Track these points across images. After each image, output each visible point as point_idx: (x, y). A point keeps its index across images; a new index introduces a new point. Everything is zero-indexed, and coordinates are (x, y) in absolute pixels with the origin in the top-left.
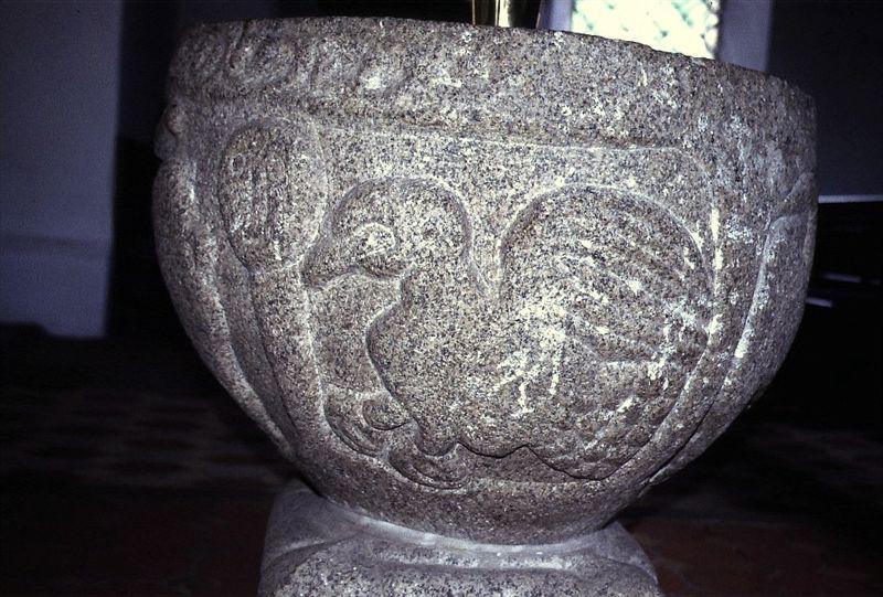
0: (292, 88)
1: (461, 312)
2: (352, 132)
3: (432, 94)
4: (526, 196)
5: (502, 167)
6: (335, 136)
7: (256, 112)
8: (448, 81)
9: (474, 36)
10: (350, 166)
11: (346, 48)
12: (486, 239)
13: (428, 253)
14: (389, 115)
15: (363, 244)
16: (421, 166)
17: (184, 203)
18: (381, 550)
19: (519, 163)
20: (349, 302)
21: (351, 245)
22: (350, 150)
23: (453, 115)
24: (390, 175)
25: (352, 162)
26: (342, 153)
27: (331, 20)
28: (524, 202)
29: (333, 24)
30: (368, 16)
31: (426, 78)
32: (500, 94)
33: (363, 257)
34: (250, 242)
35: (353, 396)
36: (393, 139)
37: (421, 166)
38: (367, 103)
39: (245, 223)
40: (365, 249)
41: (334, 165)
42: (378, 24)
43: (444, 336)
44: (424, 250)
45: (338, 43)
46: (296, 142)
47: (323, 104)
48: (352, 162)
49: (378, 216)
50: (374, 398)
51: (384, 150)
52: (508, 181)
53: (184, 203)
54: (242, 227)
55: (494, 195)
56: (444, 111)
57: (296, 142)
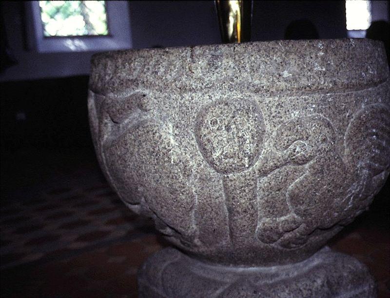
0: (240, 81)
1: (337, 172)
2: (277, 99)
3: (315, 76)
4: (353, 115)
5: (343, 104)
6: (267, 102)
7: (128, 94)
8: (319, 68)
9: (323, 45)
10: (279, 115)
11: (264, 57)
12: (340, 137)
13: (323, 149)
14: (299, 89)
15: (294, 152)
16: (312, 109)
17: (169, 146)
18: (257, 281)
19: (349, 101)
20: (282, 179)
21: (288, 153)
22: (277, 107)
23: (326, 84)
24: (298, 116)
25: (279, 113)
26: (273, 109)
27: (252, 44)
28: (352, 118)
29: (253, 46)
30: (271, 41)
31: (311, 69)
32: (341, 71)
33: (294, 157)
34: (227, 161)
35: (276, 221)
36: (298, 99)
37: (312, 109)
38: (287, 84)
39: (223, 152)
40: (295, 154)
41: (269, 116)
42: (278, 44)
43: (329, 184)
44: (322, 148)
45: (260, 56)
46: (251, 108)
47: (263, 87)
48: (279, 113)
49: (301, 137)
50: (287, 219)
51: (294, 105)
52: (346, 110)
53: (169, 146)
54: (222, 154)
55: (342, 116)
56: (322, 83)
57: (251, 108)
